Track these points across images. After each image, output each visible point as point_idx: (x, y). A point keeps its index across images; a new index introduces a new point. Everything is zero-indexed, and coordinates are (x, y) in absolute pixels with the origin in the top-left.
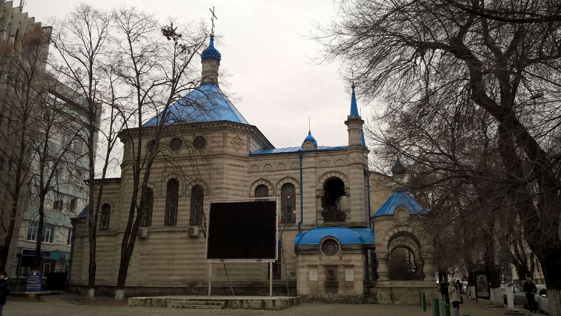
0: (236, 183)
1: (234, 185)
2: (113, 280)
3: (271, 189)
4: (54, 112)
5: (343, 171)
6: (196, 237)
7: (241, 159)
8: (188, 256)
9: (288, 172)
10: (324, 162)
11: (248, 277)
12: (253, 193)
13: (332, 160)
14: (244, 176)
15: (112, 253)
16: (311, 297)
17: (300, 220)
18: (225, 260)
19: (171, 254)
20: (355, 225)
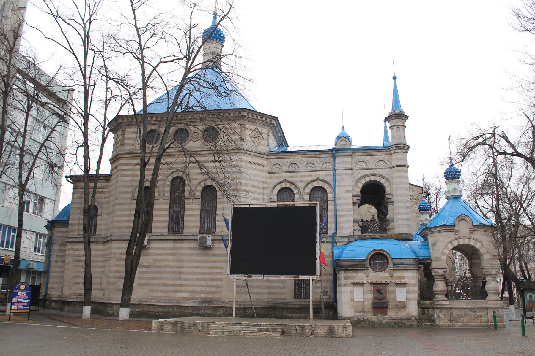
0: (256, 184)
1: (254, 186)
2: (116, 297)
3: (298, 193)
4: (34, 92)
5: (384, 174)
6: (209, 248)
7: (261, 155)
8: (199, 270)
9: (318, 173)
10: (362, 163)
11: (270, 296)
12: (275, 197)
13: (372, 161)
14: (264, 177)
15: (101, 264)
16: (356, 319)
17: (333, 231)
18: (253, 276)
19: (177, 267)
20: (400, 237)
